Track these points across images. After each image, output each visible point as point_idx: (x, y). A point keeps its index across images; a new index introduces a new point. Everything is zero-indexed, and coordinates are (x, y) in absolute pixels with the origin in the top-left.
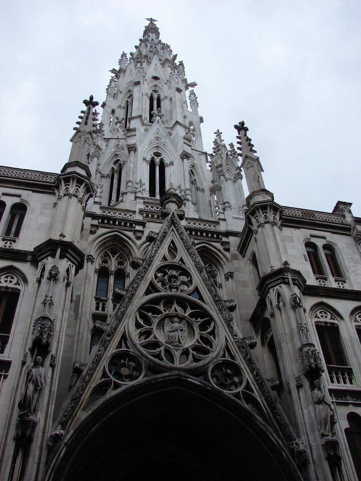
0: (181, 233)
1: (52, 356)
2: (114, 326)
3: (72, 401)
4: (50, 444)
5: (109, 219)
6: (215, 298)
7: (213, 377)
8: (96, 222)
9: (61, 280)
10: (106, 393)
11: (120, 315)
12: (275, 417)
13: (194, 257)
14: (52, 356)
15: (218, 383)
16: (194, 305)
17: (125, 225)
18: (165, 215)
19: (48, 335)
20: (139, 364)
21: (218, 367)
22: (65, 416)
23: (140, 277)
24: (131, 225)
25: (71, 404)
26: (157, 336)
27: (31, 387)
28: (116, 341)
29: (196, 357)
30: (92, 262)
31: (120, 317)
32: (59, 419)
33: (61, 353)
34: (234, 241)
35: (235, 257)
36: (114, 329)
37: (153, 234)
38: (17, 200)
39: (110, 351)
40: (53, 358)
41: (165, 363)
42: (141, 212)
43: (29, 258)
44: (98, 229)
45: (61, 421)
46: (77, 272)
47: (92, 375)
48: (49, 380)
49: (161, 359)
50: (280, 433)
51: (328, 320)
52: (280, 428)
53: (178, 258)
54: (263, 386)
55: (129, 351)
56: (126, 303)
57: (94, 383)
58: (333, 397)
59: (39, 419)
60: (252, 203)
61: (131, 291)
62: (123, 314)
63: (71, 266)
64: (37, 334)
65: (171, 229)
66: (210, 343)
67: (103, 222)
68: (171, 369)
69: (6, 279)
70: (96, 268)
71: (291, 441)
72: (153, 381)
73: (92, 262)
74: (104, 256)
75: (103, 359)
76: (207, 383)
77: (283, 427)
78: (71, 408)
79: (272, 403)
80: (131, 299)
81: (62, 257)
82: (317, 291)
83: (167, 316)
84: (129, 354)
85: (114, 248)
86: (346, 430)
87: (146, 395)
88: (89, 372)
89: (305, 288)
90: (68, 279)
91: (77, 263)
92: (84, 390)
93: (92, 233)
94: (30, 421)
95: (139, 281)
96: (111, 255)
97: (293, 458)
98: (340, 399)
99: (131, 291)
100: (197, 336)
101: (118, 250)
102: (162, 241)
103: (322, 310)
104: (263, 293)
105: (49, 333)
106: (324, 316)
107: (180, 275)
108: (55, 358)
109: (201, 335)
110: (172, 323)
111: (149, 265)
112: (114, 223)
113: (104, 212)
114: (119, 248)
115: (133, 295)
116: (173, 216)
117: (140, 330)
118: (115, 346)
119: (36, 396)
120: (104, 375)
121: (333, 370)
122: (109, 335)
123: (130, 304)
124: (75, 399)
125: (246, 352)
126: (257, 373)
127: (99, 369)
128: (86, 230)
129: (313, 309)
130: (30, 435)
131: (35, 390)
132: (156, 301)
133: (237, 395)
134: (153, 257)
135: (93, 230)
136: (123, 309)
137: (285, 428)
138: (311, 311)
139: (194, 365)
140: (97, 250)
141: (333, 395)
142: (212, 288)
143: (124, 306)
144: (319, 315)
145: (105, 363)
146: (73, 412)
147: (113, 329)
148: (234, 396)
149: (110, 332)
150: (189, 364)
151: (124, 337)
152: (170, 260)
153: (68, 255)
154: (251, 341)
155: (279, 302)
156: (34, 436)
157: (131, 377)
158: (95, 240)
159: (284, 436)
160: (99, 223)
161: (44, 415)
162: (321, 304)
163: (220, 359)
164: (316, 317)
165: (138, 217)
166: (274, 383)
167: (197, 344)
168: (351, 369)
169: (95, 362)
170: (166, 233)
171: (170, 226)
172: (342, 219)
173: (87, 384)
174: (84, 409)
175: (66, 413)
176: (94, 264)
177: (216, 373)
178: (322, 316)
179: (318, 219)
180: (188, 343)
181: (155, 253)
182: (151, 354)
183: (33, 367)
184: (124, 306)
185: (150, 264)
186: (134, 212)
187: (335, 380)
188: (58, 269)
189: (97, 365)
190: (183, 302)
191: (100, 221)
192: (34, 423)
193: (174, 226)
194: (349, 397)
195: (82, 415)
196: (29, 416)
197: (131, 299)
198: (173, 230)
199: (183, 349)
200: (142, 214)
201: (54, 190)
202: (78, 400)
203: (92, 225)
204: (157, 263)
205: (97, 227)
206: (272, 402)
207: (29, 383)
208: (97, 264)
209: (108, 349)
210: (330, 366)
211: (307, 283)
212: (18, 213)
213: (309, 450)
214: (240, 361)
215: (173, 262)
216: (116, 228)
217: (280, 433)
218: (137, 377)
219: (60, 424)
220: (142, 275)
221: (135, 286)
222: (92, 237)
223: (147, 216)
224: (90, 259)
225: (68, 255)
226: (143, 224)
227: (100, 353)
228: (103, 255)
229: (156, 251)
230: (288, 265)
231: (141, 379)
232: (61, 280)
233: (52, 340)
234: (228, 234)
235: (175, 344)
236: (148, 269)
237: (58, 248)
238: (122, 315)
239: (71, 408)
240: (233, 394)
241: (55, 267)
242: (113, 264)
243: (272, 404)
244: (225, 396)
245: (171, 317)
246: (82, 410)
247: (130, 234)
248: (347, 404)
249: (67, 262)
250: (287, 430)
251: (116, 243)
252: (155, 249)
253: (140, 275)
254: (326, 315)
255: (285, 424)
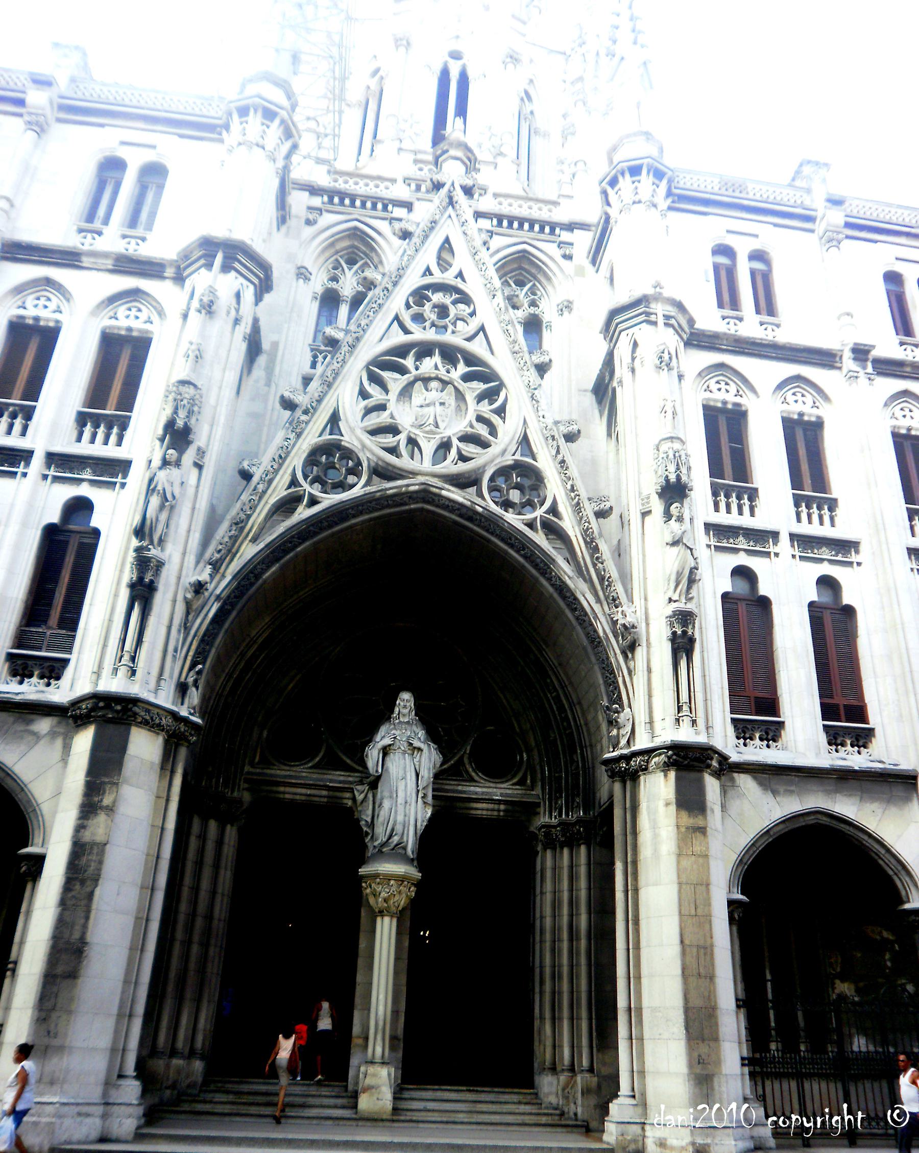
0: (463, 223)
1: (199, 449)
2: (316, 395)
3: (231, 526)
4: (189, 596)
5: (342, 195)
6: (514, 347)
7: (491, 489)
8: (317, 201)
9: (223, 313)
10: (293, 513)
11: (329, 376)
12: (594, 565)
13: (484, 269)
14: (199, 449)
15: (501, 500)
16: (471, 359)
17: (374, 207)
18: (437, 186)
19: (189, 413)
20: (359, 463)
21: (504, 472)
22: (219, 551)
23: (374, 305)
24: (385, 208)
25: (230, 531)
26: (395, 414)
27: (155, 501)
28: (320, 421)
29: (463, 452)
30: (307, 279)
31: (330, 379)
32: (207, 555)
33: (217, 444)
34: (582, 241)
35: (580, 271)
36: (317, 401)
37: (410, 223)
38: (149, 156)
39: (307, 441)
40: (201, 452)
41: (404, 462)
42: (407, 181)
43: (170, 272)
44: (321, 214)
45: (211, 558)
46: (258, 298)
47: (270, 482)
48: (191, 491)
49: (398, 456)
50: (601, 593)
51: (731, 398)
52: (602, 583)
53: (453, 271)
54: (580, 509)
55: (341, 440)
56: (343, 353)
57: (274, 495)
58: (711, 536)
59: (170, 556)
60: (616, 160)
61: (355, 333)
62: (336, 374)
63: (245, 286)
64: (169, 411)
65: (446, 215)
66: (493, 431)
67: (331, 201)
68: (414, 474)
69: (128, 312)
70: (316, 291)
71: (617, 607)
72: (378, 494)
73: (306, 279)
74: (335, 268)
75: (292, 454)
76: (479, 501)
77: (606, 583)
78: (230, 537)
79: (592, 540)
80: (354, 346)
81: (226, 268)
82: (716, 342)
83: (417, 379)
84: (340, 445)
85: (354, 253)
86: (725, 596)
87: (366, 517)
88: (264, 476)
89: (692, 334)
90: (237, 311)
91: (256, 281)
92: (253, 508)
93: (309, 222)
94: (152, 558)
95: (371, 314)
96: (345, 266)
97: (616, 637)
98: (725, 541)
99: (355, 333)
100: (471, 416)
101: (360, 256)
102: (426, 237)
103: (721, 378)
104: (611, 340)
105: (189, 410)
106: (723, 390)
107: (454, 303)
108: (204, 453)
109: (480, 413)
110: (427, 390)
111: (395, 284)
112: (353, 204)
113: (336, 181)
114: (362, 253)
115: (358, 339)
116: (452, 189)
117: (366, 402)
118: (316, 432)
119: (163, 516)
120: (294, 482)
121: (722, 489)
122: (306, 412)
123: (350, 356)
124: (236, 524)
125: (558, 447)
126: (572, 486)
127: (285, 472)
128: (297, 217)
129: (703, 375)
130: (152, 582)
131: (162, 507)
132: (402, 351)
133: (531, 525)
134: (403, 269)
135: (311, 217)
136: (336, 364)
137: (609, 585)
138: (699, 379)
139: (462, 467)
140: (319, 256)
141: (711, 533)
142: (509, 327)
143: (339, 360)
144: (714, 387)
145: (297, 460)
146: (233, 545)
147: (314, 400)
148: (526, 524)
149: (309, 406)
150: (450, 466)
151: (334, 419)
152: (438, 277)
153: (237, 265)
154: (570, 429)
155: (633, 359)
156: (158, 583)
157: (342, 486)
158: (314, 237)
159: (607, 598)
160: (323, 203)
161: (180, 548)
162: (722, 366)
163: (509, 460)
164: (708, 389)
165: (401, 192)
166: (602, 506)
167: (469, 429)
168: (756, 490)
169: (277, 460)
170: (435, 222)
171: (445, 209)
172: (805, 195)
173: (260, 498)
174: (254, 540)
175: (220, 547)
176: (312, 283)
177: (498, 483)
178: (719, 390)
179: (751, 196)
180: (454, 427)
181: (408, 260)
182: (382, 445)
183: (160, 468)
184: (339, 360)
185: (396, 282)
186: (393, 181)
187: (723, 506)
188: (216, 293)
189: (281, 465)
190: (450, 354)
191: (326, 198)
192: (158, 561)
193: (453, 207)
194: (741, 538)
195: (248, 551)
196: (149, 550)
197: (353, 347)
198: (450, 216)
199: (442, 438)
200: (409, 185)
201: (220, 134)
202: (243, 524)
203: (310, 209)
204: (413, 280)
205: (320, 211)
206: (593, 538)
207: (152, 495)
208: (319, 282)
209: (303, 436)
210: (718, 483)
211: (696, 326)
212: (112, 178)
213: (644, 625)
214: (545, 463)
215: (443, 278)
216: (357, 212)
217: (601, 593)
218: (352, 486)
219: (210, 564)
220: (379, 302)
221: (363, 323)
222: (309, 231)
223: (418, 188)
224: (302, 274)
225: (237, 265)
226: (409, 206)
227: (286, 443)
228: (330, 267)
229: (412, 258)
230: (661, 288)
231: (357, 492)
232: (223, 313)
233: (197, 420)
234: (570, 227)
235: (428, 429)
236: (393, 290)
237: (217, 252)
238: (333, 375)
239: (230, 537)
240: (525, 522)
241: (212, 291)
242: (348, 283)
243: (592, 542)
244: (506, 524)
245: (426, 380)
246: (250, 541)
247: (383, 226)
248: (736, 551)
249: (236, 278)
250: (613, 588)
251: (356, 243)
252: (409, 252)
253: (376, 302)
254: (727, 387)
255: (609, 577)
